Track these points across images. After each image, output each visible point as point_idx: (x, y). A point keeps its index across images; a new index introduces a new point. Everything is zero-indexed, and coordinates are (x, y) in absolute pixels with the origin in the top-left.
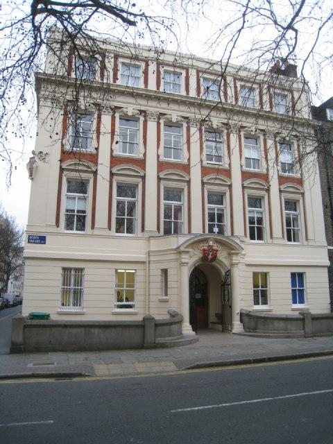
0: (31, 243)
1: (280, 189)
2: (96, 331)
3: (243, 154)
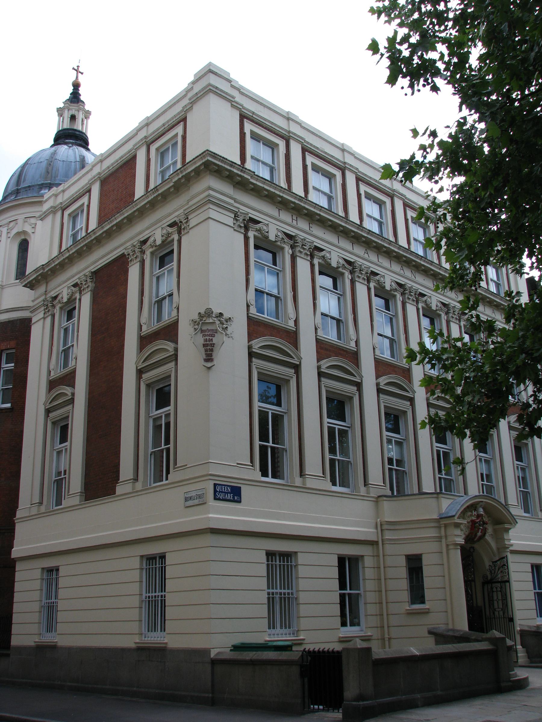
0: (219, 499)
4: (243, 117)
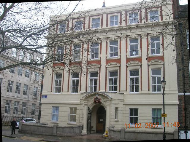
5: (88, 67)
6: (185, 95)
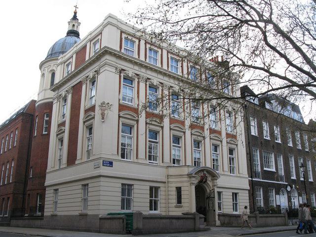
1: (119, 114)
2: (174, 221)
3: (121, 91)
4: (122, 32)
5: (148, 122)
6: (252, 180)
